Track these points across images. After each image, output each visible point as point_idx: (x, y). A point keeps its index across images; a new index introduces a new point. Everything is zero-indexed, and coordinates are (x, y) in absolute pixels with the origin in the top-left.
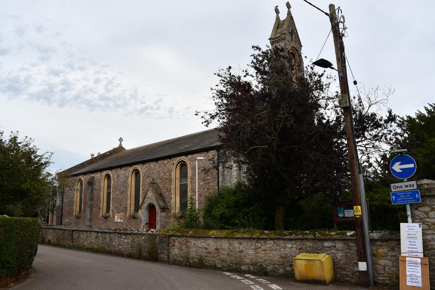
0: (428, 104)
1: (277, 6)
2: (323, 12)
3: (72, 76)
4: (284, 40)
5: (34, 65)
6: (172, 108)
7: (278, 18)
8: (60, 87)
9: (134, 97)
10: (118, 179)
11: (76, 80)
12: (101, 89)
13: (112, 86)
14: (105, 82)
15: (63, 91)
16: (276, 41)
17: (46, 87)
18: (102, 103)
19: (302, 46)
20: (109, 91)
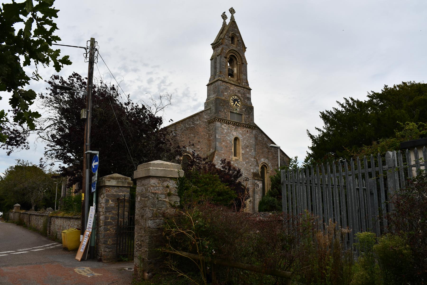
1: (225, 12)
2: (80, 47)
4: (222, 44)
7: (224, 23)
9: (186, 95)
10: (342, 176)
11: (131, 81)
13: (164, 85)
14: (158, 82)
16: (216, 46)
19: (246, 48)
20: (162, 91)
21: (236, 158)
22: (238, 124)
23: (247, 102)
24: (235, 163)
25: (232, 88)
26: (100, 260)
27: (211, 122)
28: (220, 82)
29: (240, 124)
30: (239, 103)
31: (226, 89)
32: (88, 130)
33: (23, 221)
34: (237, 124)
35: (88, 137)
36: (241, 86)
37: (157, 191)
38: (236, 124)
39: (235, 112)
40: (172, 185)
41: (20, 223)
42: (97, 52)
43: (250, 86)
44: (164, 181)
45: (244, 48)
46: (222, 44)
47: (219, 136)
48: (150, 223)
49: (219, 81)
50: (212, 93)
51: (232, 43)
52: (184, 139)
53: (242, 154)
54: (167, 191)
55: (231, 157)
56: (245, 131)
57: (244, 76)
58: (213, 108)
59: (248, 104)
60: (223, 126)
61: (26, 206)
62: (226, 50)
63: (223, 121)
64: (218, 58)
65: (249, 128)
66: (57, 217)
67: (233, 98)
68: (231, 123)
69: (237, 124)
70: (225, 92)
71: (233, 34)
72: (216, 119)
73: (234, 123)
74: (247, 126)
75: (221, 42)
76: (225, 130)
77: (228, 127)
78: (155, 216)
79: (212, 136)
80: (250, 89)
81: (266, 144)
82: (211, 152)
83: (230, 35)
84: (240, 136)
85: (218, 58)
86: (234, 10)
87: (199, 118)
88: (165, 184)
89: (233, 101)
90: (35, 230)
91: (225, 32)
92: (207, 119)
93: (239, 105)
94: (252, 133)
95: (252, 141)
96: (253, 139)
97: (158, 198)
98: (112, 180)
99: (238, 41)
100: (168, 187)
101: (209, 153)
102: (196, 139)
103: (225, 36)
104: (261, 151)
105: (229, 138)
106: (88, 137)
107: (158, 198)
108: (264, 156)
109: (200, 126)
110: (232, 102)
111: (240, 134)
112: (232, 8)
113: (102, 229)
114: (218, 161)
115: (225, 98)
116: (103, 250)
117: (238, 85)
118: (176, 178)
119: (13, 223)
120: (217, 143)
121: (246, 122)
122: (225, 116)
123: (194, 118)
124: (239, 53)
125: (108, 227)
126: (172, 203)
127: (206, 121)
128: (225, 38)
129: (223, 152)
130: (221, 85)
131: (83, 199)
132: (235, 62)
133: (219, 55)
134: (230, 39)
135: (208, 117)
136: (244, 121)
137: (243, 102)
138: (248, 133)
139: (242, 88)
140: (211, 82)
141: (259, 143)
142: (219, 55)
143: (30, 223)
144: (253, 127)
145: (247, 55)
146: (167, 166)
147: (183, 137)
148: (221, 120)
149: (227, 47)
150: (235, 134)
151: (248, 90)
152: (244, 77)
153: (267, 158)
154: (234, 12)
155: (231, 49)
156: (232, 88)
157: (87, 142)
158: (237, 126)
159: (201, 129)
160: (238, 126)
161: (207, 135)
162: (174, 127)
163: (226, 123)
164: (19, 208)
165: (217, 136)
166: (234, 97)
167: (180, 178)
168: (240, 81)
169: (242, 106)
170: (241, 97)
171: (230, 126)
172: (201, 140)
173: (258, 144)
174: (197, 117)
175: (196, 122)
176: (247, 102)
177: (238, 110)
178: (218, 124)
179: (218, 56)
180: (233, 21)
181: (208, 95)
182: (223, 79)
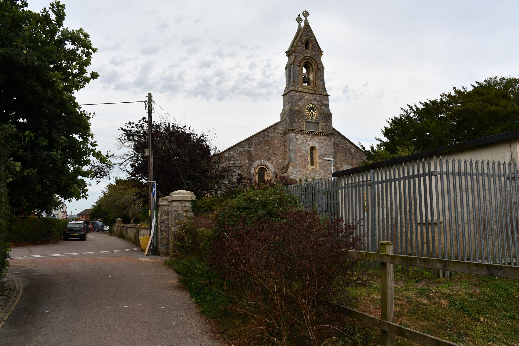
0: (386, 120)
2: (141, 102)
3: (226, 64)
5: (184, 59)
6: (346, 86)
7: (299, 27)
8: (216, 79)
11: (229, 69)
12: (258, 76)
15: (219, 83)
17: (201, 82)
18: (264, 91)
19: (323, 52)
21: (313, 167)
22: (314, 133)
23: (324, 109)
24: (312, 172)
25: (306, 97)
26: (159, 255)
27: (285, 133)
28: (293, 92)
29: (316, 133)
30: (315, 111)
31: (301, 98)
32: (151, 164)
33: (123, 234)
34: (313, 133)
35: (151, 169)
36: (318, 93)
37: (178, 209)
38: (312, 133)
39: (310, 121)
40: (188, 205)
41: (121, 236)
42: (153, 103)
43: (328, 92)
44: (182, 203)
45: (321, 53)
46: (295, 52)
47: (293, 147)
48: (173, 229)
49: (292, 91)
50: (287, 103)
51: (306, 49)
52: (259, 152)
53: (319, 162)
54: (184, 209)
55: (307, 167)
56: (322, 139)
57: (321, 82)
58: (287, 119)
59: (326, 111)
60: (297, 137)
61: (126, 220)
62: (299, 58)
63: (297, 131)
64: (292, 67)
65: (327, 136)
66: (142, 228)
67: (308, 107)
68: (306, 133)
69: (313, 133)
70: (299, 102)
71: (307, 39)
72: (290, 131)
73: (310, 133)
74: (325, 134)
75: (294, 50)
76: (300, 141)
77: (304, 137)
78: (178, 224)
79: (287, 147)
80: (328, 96)
81: (349, 150)
82: (286, 163)
83: (304, 41)
84: (317, 145)
85: (292, 67)
86: (307, 12)
87: (274, 130)
88: (183, 205)
89: (308, 110)
90: (129, 240)
91: (298, 39)
92: (282, 130)
93: (315, 113)
94: (330, 141)
95: (331, 149)
96: (332, 147)
97: (178, 214)
98: (164, 201)
99: (313, 45)
100: (185, 206)
101: (285, 164)
102: (271, 151)
103: (297, 43)
104: (344, 158)
105: (304, 148)
106: (151, 169)
107: (178, 214)
108: (347, 163)
109: (275, 138)
110: (307, 111)
111: (317, 143)
112: (305, 11)
113: (159, 234)
114: (293, 172)
115: (300, 108)
116: (161, 249)
117: (314, 92)
118: (190, 201)
119: (116, 236)
120: (292, 154)
121: (322, 130)
122: (300, 126)
123: (268, 131)
124: (314, 58)
125: (163, 233)
126: (189, 216)
127: (282, 132)
128: (298, 45)
129: (298, 162)
130: (294, 95)
131: (150, 214)
132: (311, 68)
133: (292, 64)
134: (304, 45)
135: (283, 128)
136: (321, 129)
137: (320, 109)
138: (325, 141)
139: (319, 95)
140: (286, 92)
141: (341, 150)
142: (292, 64)
143: (127, 235)
144: (331, 135)
145: (323, 59)
146: (184, 194)
147: (258, 151)
148: (294, 131)
149: (300, 55)
150: (311, 143)
151: (325, 97)
152: (321, 83)
153: (350, 165)
154: (308, 15)
155: (305, 56)
156: (307, 96)
157: (150, 173)
158: (313, 135)
159: (276, 141)
160: (314, 135)
161: (283, 146)
162: (248, 141)
163: (301, 133)
164: (121, 222)
165: (291, 148)
166: (309, 106)
167: (193, 201)
168: (317, 88)
169: (318, 114)
170: (318, 104)
171: (305, 135)
172: (276, 152)
173: (340, 151)
174: (272, 130)
175: (270, 135)
176: (324, 109)
177: (314, 118)
178: (292, 135)
179: (291, 65)
180: (307, 26)
181: (284, 106)
182: (296, 89)
